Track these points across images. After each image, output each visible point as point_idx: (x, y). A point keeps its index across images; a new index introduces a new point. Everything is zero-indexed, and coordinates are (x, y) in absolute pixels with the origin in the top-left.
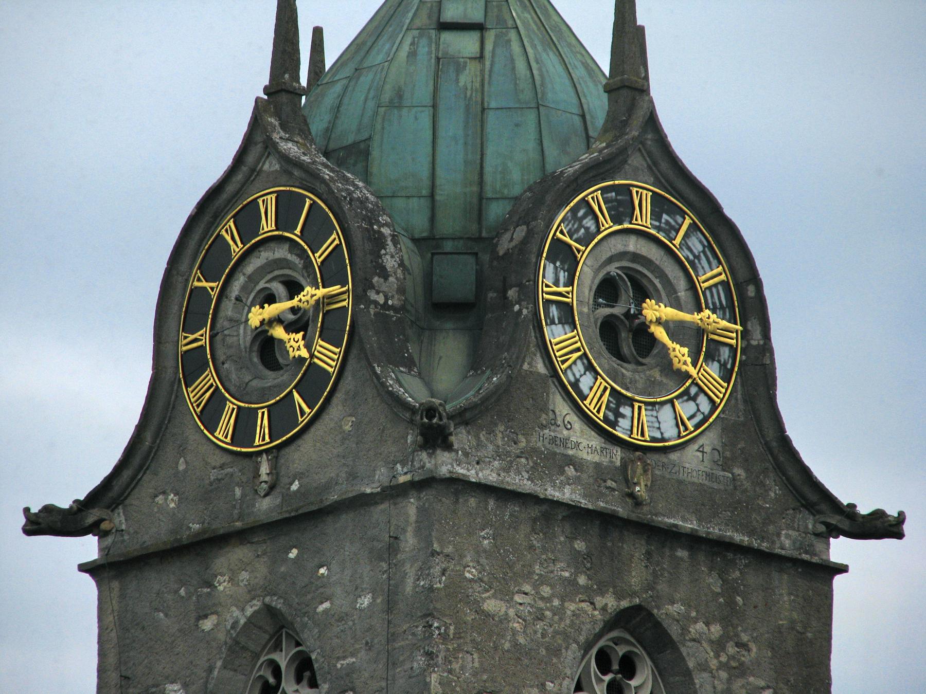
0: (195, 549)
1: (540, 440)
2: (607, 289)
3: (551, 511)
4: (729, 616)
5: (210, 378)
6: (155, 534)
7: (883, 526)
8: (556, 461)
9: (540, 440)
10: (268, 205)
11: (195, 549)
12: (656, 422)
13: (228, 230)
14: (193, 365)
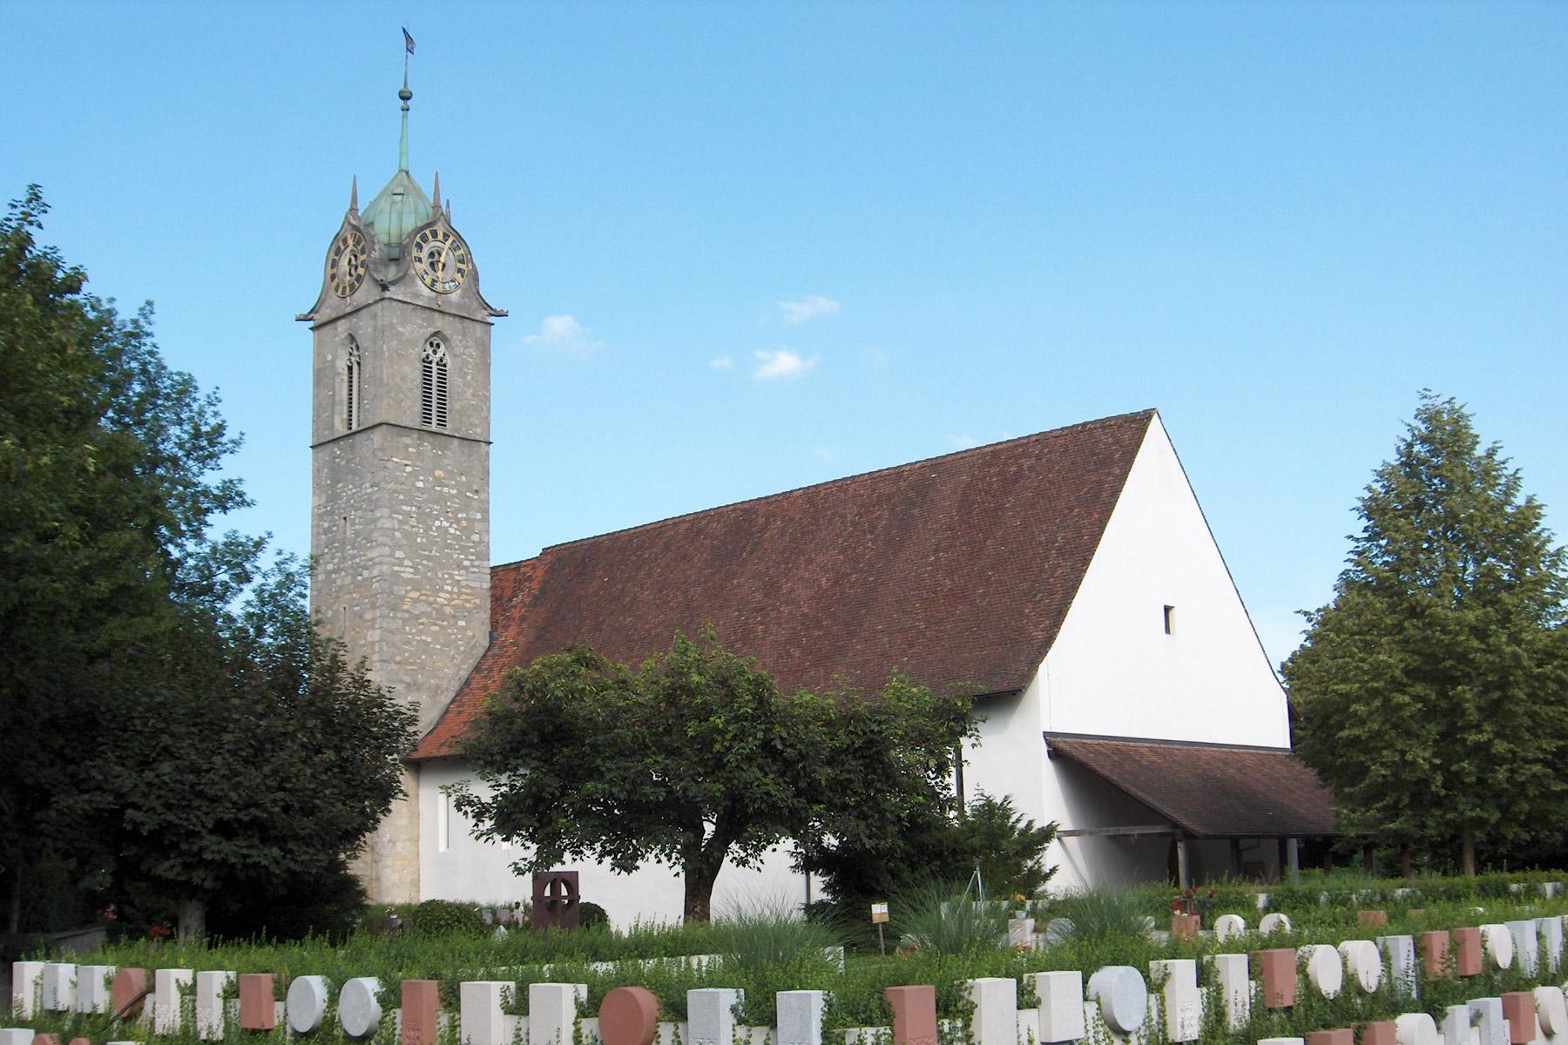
4: (464, 334)
8: (417, 295)
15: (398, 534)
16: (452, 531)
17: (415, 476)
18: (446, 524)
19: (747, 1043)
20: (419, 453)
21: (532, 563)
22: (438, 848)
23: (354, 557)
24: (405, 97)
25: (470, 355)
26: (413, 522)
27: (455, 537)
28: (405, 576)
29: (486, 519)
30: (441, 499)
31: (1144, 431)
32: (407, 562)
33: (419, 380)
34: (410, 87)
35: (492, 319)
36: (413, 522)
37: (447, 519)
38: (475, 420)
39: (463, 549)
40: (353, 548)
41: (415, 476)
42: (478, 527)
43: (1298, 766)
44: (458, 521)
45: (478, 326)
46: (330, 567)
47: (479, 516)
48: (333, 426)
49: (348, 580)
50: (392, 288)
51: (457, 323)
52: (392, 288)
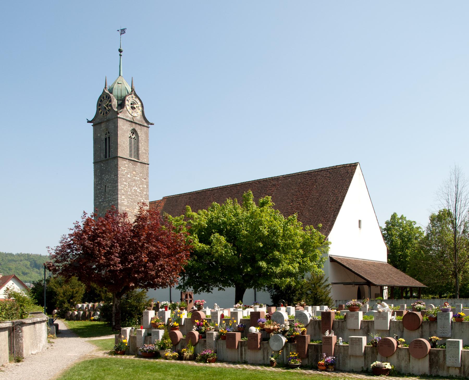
0: (100, 123)
1: (126, 115)
2: (131, 104)
3: (127, 120)
4: (141, 130)
5: (101, 110)
6: (97, 122)
7: (152, 124)
8: (128, 117)
9: (126, 115)
10: (105, 96)
11: (100, 123)
12: (135, 115)
13: (102, 99)
14: (100, 109)
15: (123, 191)
16: (138, 191)
17: (127, 173)
18: (136, 188)
20: (128, 166)
21: (159, 202)
24: (120, 51)
26: (127, 187)
27: (139, 193)
28: (125, 204)
30: (135, 180)
31: (355, 169)
32: (125, 200)
35: (149, 126)
36: (127, 187)
37: (136, 187)
38: (144, 157)
39: (141, 197)
41: (127, 173)
42: (145, 190)
43: (390, 267)
44: (140, 188)
45: (145, 128)
47: (146, 186)
48: (100, 157)
50: (120, 114)
51: (139, 127)
52: (120, 114)
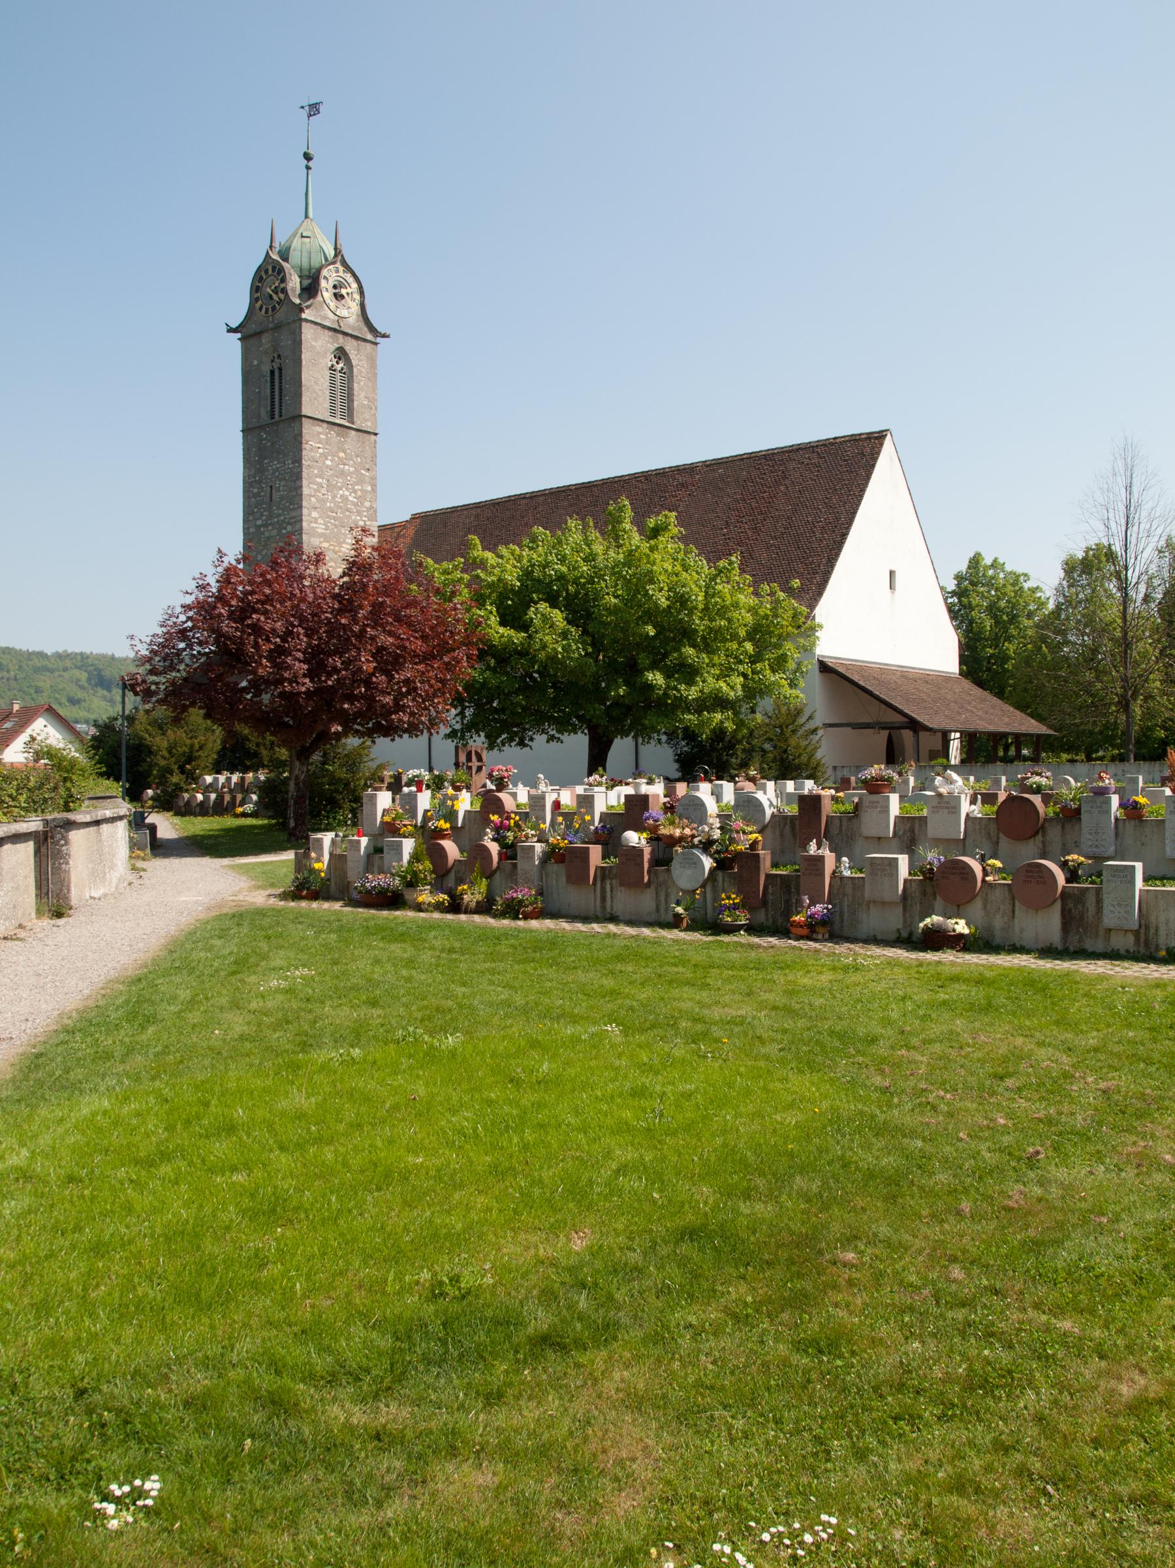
4: (358, 350)
8: (325, 318)
16: (351, 498)
19: (1174, 1170)
20: (327, 438)
21: (403, 526)
22: (436, 773)
23: (279, 515)
24: (308, 157)
25: (363, 366)
26: (324, 491)
29: (374, 490)
30: (342, 474)
31: (882, 445)
32: (320, 521)
33: (327, 384)
34: (310, 151)
35: (379, 340)
36: (324, 491)
37: (347, 489)
38: (367, 416)
40: (279, 508)
42: (369, 497)
44: (355, 492)
45: (368, 345)
46: (259, 522)
47: (369, 488)
49: (275, 532)
51: (354, 343)
